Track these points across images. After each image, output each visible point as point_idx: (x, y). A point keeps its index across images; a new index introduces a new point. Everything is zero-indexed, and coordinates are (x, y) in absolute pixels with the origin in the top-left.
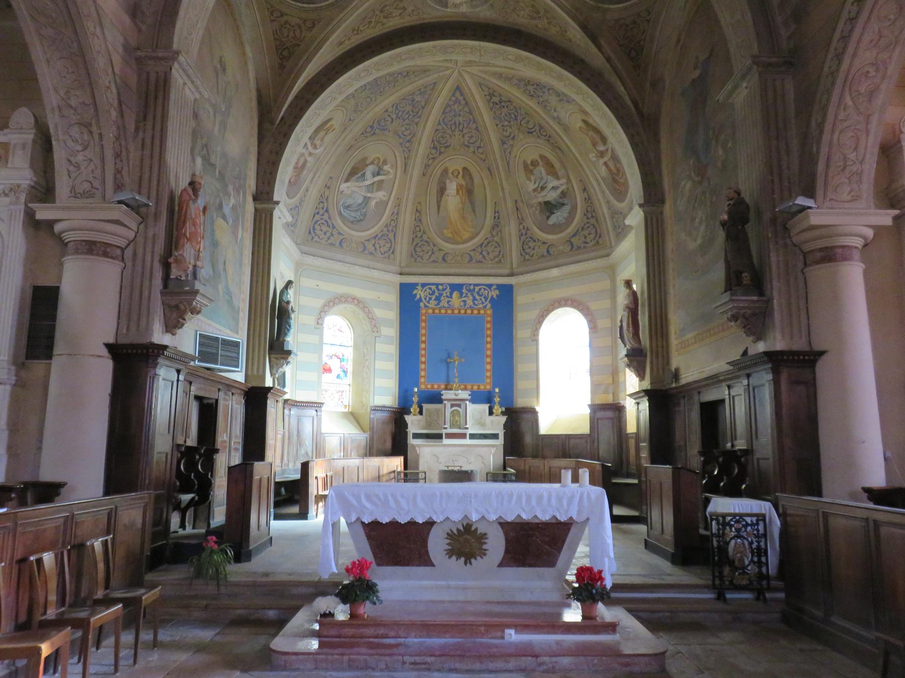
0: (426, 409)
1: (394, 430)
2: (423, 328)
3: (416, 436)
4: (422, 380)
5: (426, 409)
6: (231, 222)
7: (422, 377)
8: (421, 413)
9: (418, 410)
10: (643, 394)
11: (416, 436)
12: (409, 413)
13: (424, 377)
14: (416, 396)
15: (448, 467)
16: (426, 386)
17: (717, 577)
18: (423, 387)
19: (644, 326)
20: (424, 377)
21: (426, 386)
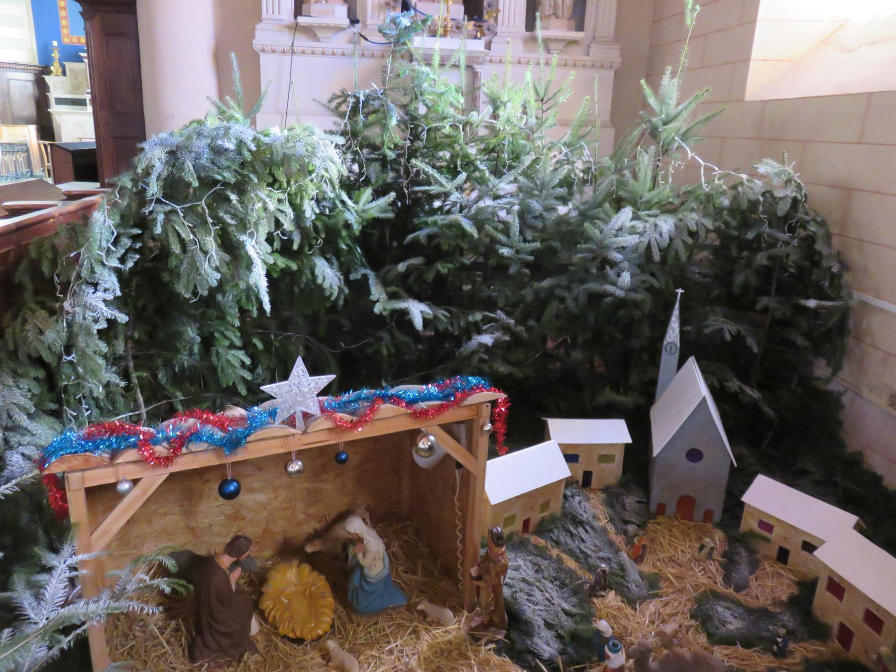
0: (71, 69)
1: (37, 92)
2: (62, 8)
3: (60, 101)
4: (65, 31)
5: (71, 69)
6: (464, 441)
7: (64, 27)
8: (64, 73)
9: (60, 70)
10: (321, 40)
11: (60, 101)
12: (49, 73)
13: (67, 27)
14: (56, 52)
15: (81, 139)
16: (71, 39)
17: (87, 460)
18: (66, 40)
19: (106, 532)
20: (67, 27)
21: (71, 39)
